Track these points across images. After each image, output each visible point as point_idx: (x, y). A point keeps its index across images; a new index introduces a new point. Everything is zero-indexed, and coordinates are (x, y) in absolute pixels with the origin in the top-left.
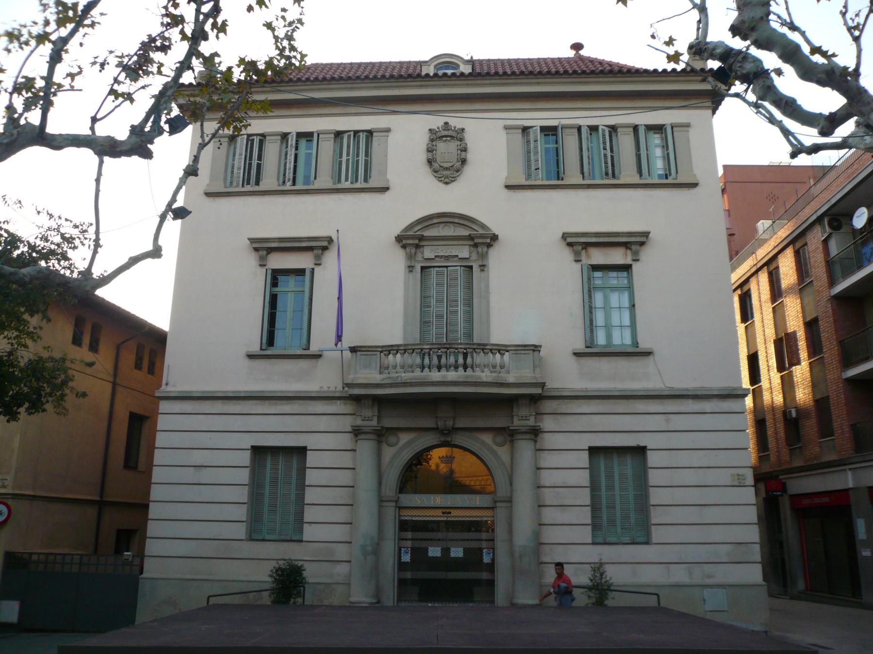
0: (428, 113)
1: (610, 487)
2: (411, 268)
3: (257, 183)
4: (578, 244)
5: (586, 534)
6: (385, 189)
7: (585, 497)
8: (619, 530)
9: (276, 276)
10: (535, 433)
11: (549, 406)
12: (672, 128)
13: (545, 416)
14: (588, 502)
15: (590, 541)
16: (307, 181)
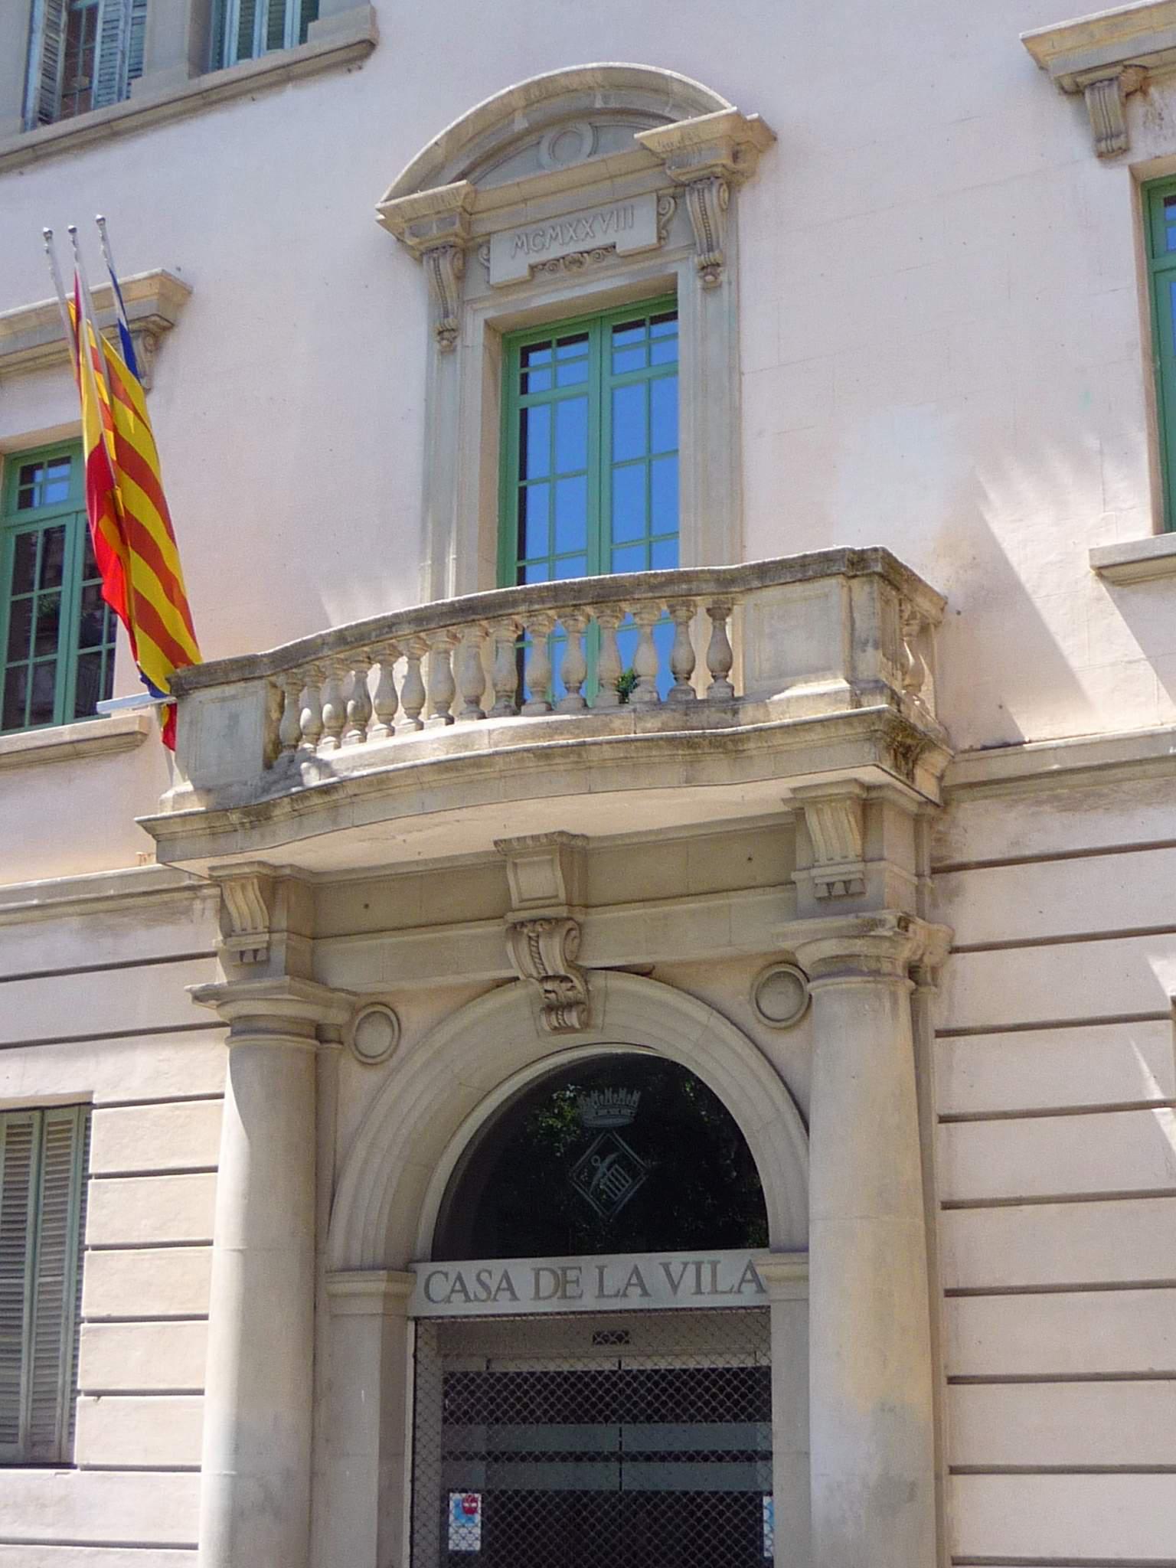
2: (446, 335)
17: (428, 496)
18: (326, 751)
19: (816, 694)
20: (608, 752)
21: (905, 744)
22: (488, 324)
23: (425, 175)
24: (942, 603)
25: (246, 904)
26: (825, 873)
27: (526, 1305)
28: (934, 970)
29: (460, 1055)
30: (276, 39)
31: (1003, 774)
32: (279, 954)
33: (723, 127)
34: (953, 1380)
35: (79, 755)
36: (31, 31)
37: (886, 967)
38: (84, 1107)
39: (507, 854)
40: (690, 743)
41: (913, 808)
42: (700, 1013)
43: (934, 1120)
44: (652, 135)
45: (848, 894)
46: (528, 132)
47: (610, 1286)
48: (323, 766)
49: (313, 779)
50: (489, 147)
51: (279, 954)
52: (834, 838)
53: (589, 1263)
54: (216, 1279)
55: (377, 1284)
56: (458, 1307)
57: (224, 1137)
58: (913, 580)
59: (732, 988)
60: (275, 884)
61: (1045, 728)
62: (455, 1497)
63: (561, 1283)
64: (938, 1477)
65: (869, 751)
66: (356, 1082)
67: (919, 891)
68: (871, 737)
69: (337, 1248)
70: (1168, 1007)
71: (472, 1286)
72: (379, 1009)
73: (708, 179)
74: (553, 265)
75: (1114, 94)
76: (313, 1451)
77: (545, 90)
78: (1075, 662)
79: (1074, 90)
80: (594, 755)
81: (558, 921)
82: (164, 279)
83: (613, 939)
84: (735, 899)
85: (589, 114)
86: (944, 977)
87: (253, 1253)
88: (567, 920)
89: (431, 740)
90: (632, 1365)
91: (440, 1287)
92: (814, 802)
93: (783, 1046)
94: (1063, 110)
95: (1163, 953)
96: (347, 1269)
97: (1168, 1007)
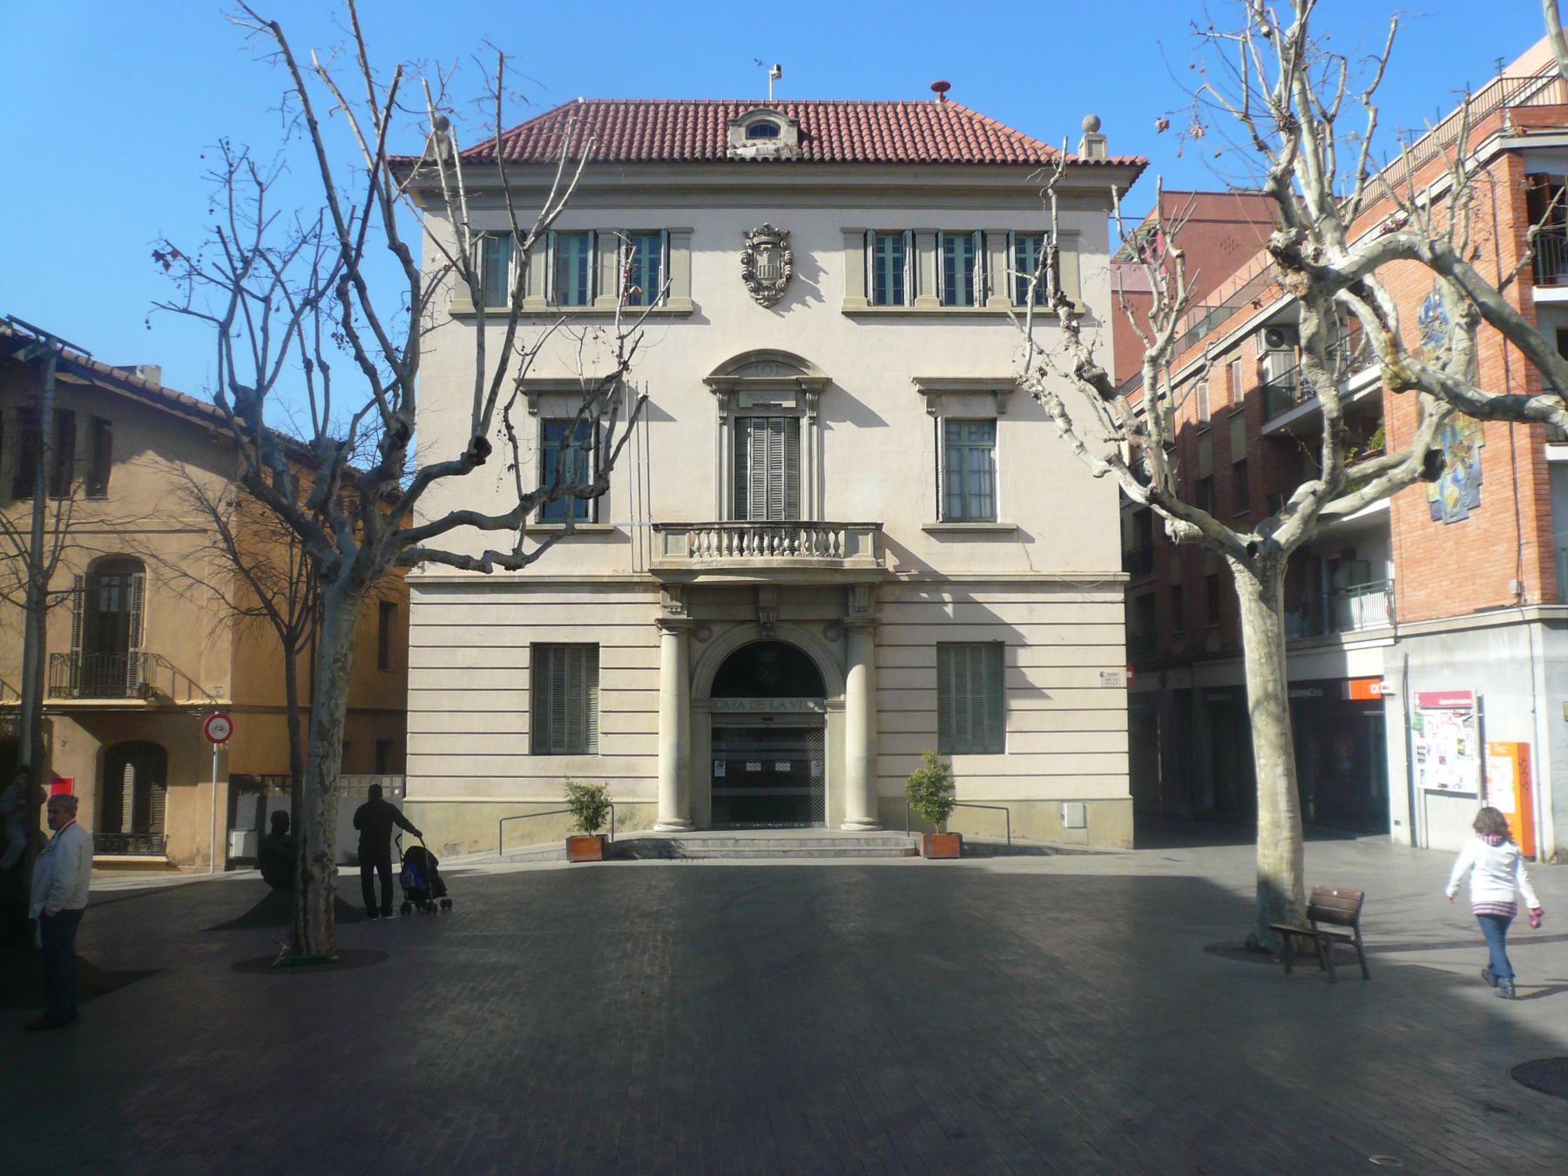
0: (837, 207)
1: (961, 689)
3: (582, 300)
4: (935, 391)
5: (524, 744)
7: (932, 701)
8: (970, 737)
10: (875, 625)
11: (890, 594)
12: (914, 236)
14: (935, 706)
23: (722, 368)
50: (744, 362)
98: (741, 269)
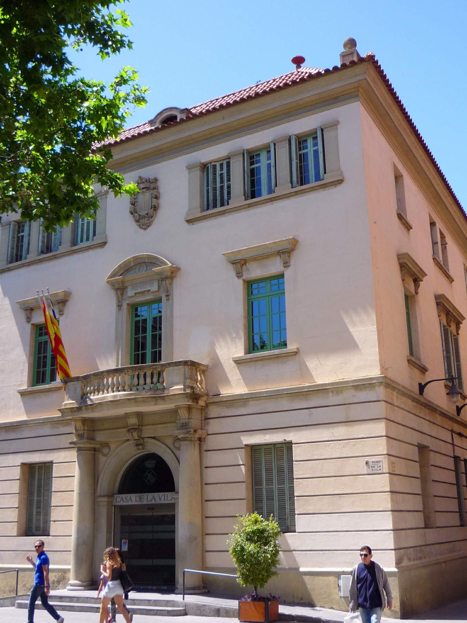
1: (269, 481)
2: (119, 306)
6: (341, 182)
9: (249, 285)
12: (322, 130)
13: (211, 420)
15: (459, 524)
16: (270, 191)
17: (116, 339)
18: (92, 397)
19: (178, 388)
20: (140, 399)
21: (195, 397)
22: (128, 304)
23: (113, 275)
24: (207, 366)
25: (79, 424)
26: (182, 421)
27: (134, 503)
28: (204, 438)
29: (121, 455)
30: (88, 239)
31: (216, 401)
32: (86, 435)
33: (169, 268)
34: (206, 517)
35: (50, 391)
36: (39, 233)
37: (193, 439)
38: (52, 463)
39: (127, 416)
40: (155, 397)
41: (200, 407)
42: (164, 446)
43: (203, 467)
44: (156, 269)
45: (186, 425)
46: (134, 265)
47: (149, 499)
48: (91, 400)
49: (89, 403)
50: (127, 269)
51: (86, 435)
52: (183, 414)
53: (145, 495)
54: (74, 498)
55: (105, 499)
56: (122, 503)
57: (76, 470)
58: (199, 364)
59: (169, 442)
60: (84, 421)
61: (226, 392)
62: (123, 540)
63: (140, 499)
64: (202, 536)
65: (186, 399)
66: (102, 459)
67: (202, 423)
68: (187, 397)
69: (99, 492)
70: (244, 446)
71: (124, 498)
72: (106, 445)
73: (166, 278)
74: (139, 293)
75: (239, 265)
76: (94, 532)
77: (136, 258)
78: (230, 379)
79: (234, 263)
80: (138, 400)
81: (136, 429)
82: (65, 292)
83: (148, 432)
84: (169, 425)
85: (145, 263)
86: (206, 439)
87: (80, 494)
88: (138, 428)
89: (109, 395)
90: (155, 514)
91: (119, 499)
92: (179, 408)
93: (177, 453)
94: (231, 267)
95: (243, 436)
96: (100, 496)
97: (244, 446)
98: (128, 206)
